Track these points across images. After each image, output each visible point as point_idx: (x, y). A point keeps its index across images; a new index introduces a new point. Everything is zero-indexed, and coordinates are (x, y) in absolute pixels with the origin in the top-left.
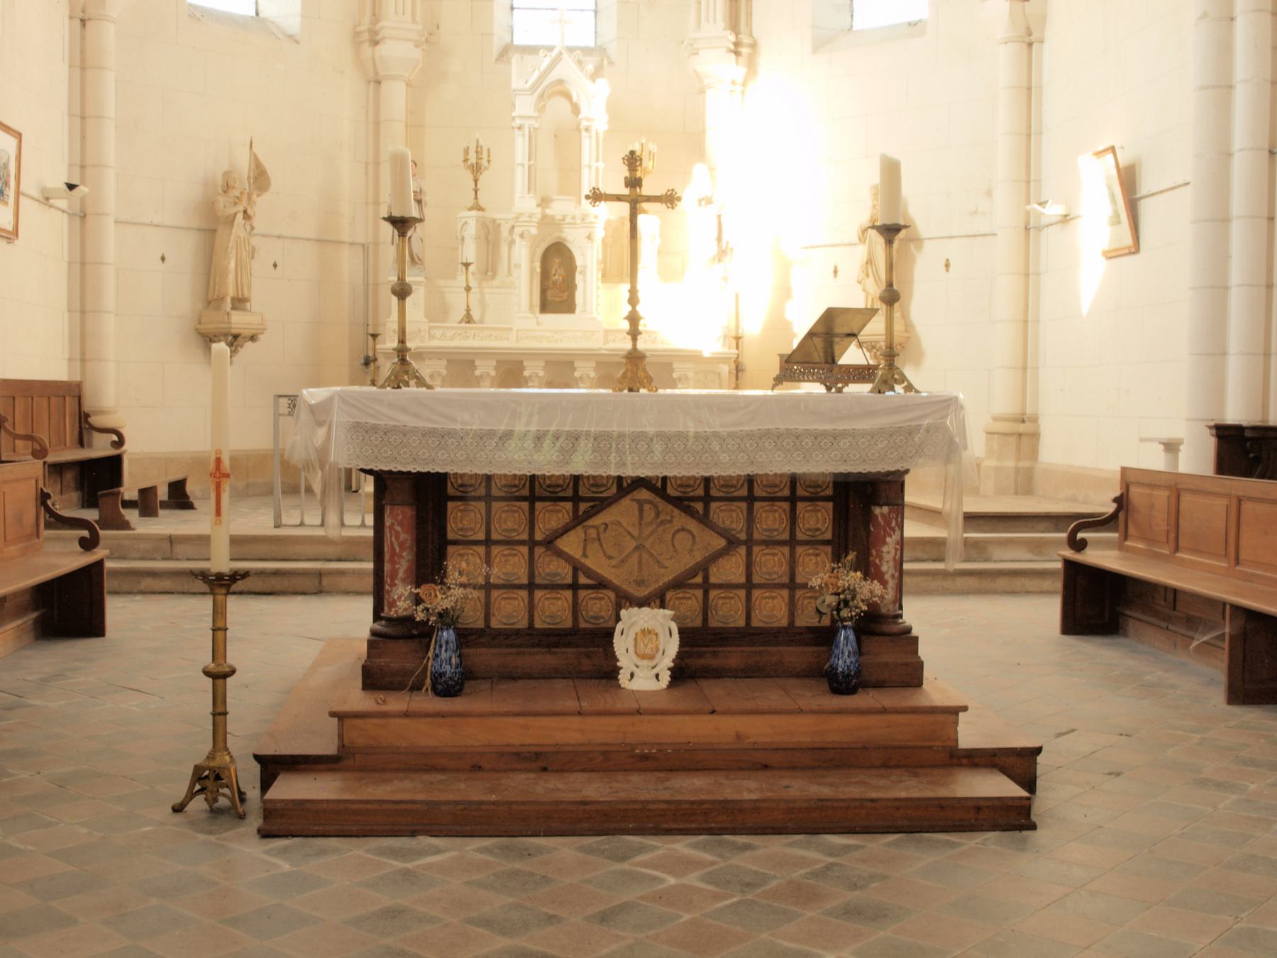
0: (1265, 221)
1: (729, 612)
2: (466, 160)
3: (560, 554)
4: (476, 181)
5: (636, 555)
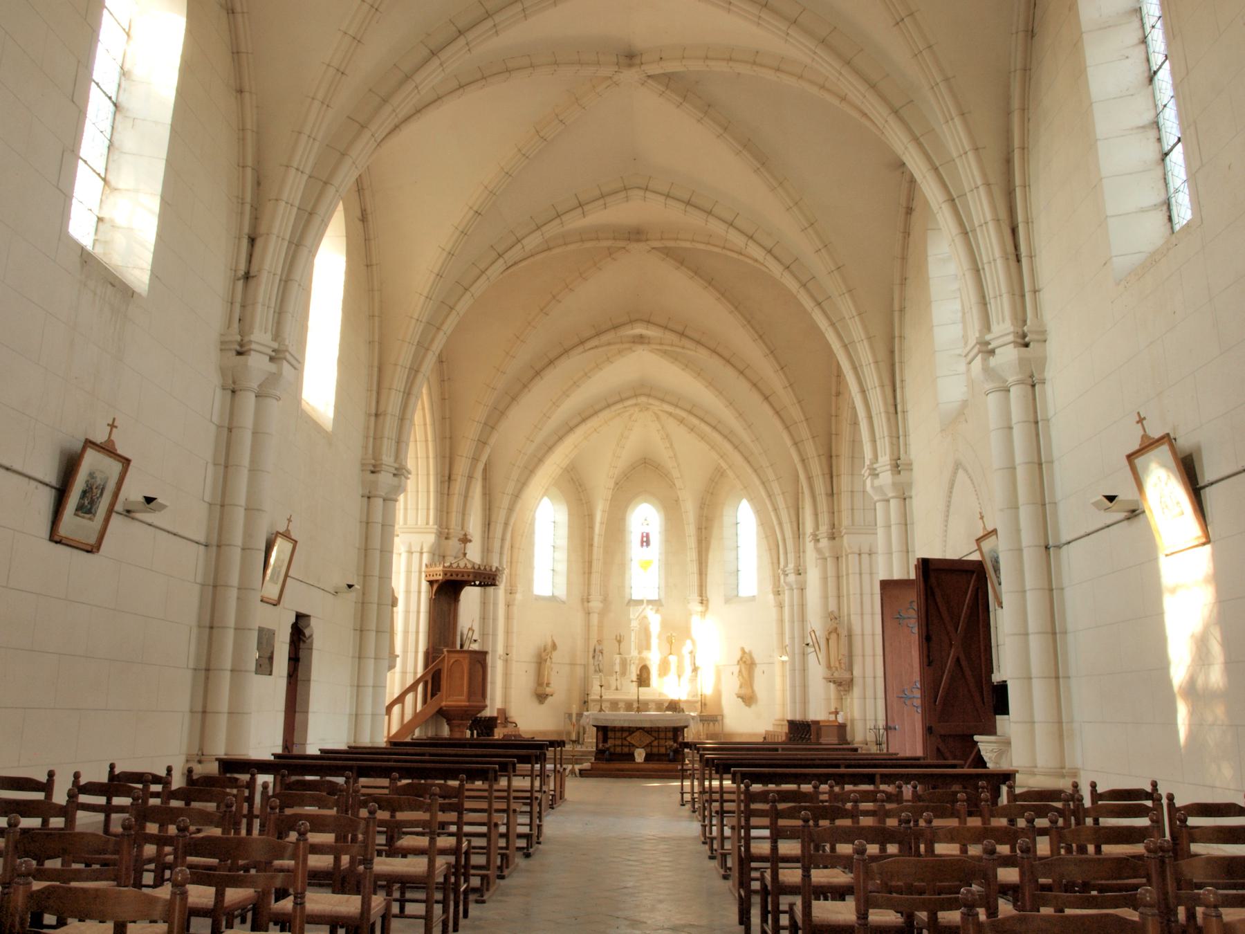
1: (655, 750)
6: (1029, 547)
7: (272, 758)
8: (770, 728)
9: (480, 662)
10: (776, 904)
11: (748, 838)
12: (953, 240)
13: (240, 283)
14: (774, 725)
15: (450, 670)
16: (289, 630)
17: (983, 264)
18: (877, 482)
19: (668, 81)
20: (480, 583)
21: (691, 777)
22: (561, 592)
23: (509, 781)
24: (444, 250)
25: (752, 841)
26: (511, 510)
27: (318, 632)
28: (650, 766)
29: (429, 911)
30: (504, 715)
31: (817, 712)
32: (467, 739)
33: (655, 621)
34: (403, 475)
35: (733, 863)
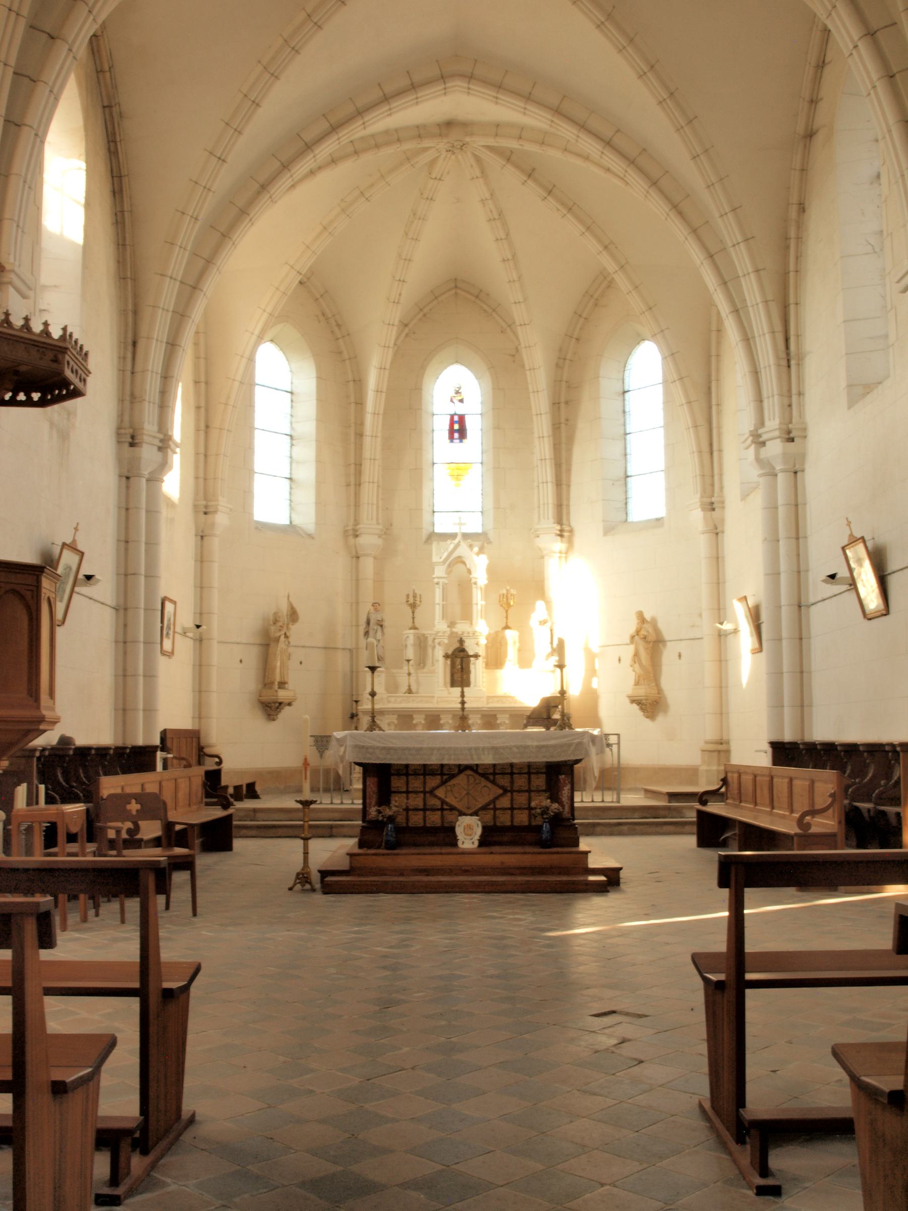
0: (798, 640)
1: (504, 819)
2: (408, 601)
3: (436, 796)
4: (413, 613)
5: (466, 797)
9: (22, 597)
22: (306, 519)
28: (497, 857)
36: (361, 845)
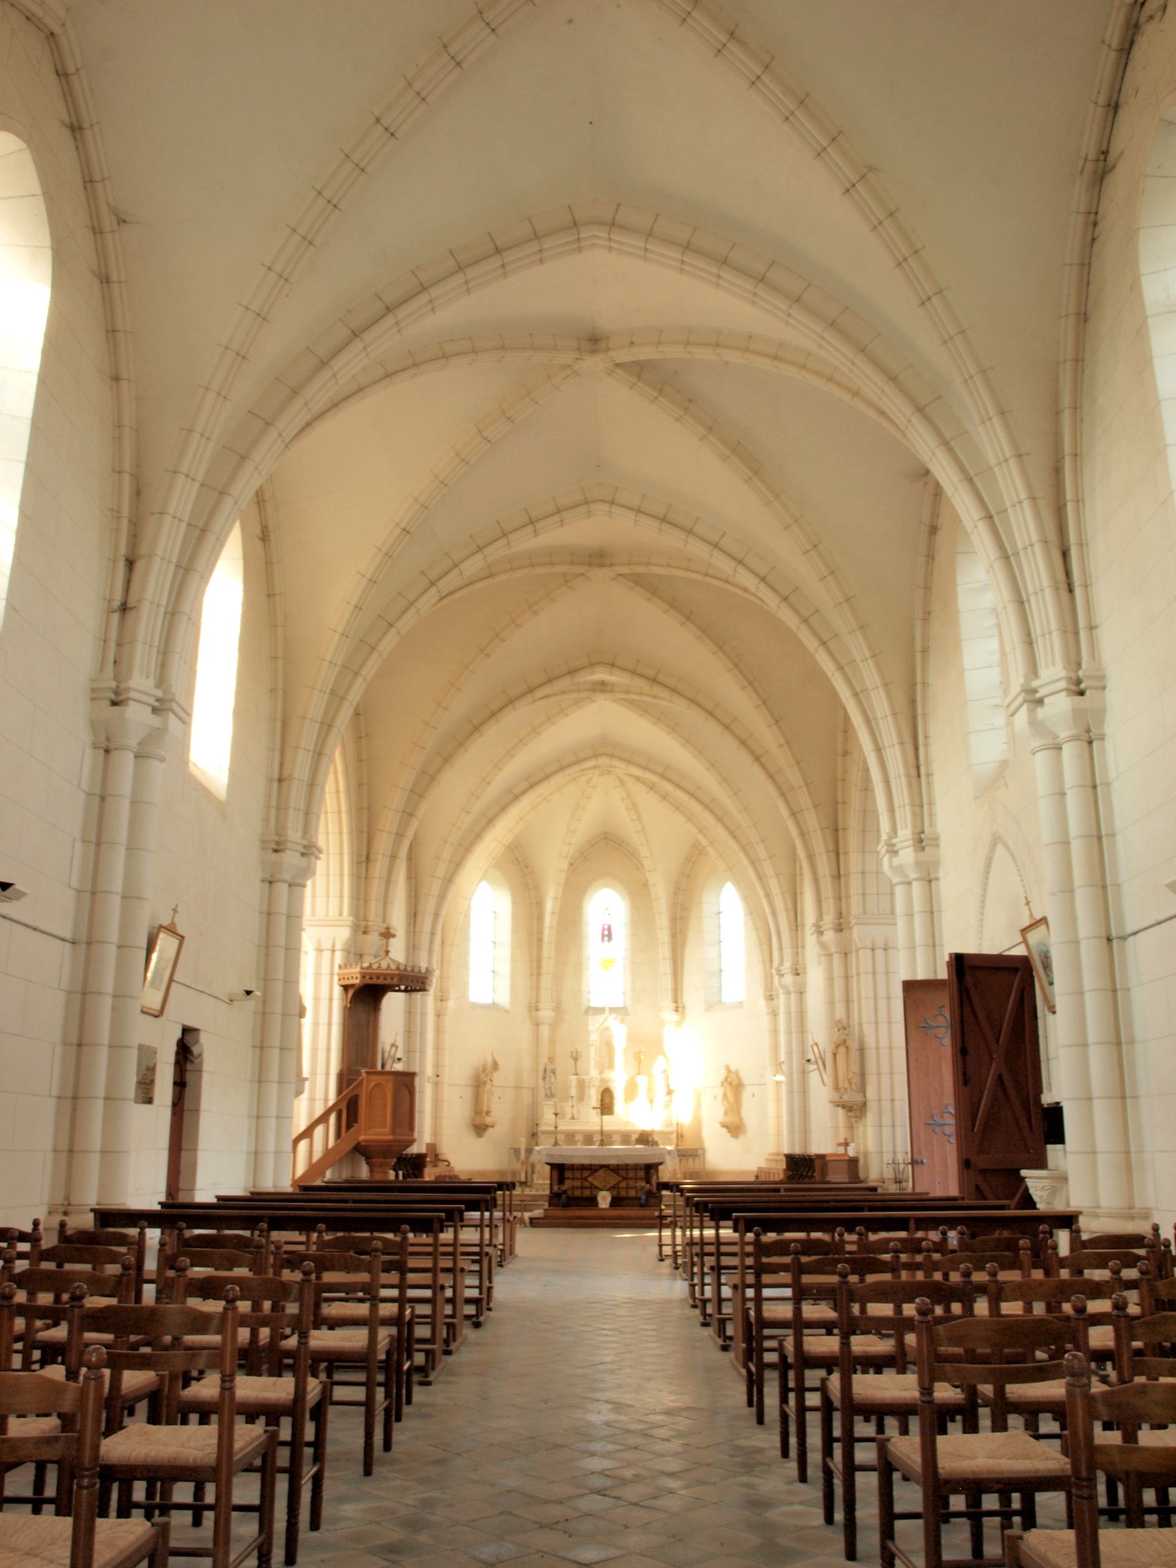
1: (623, 1193)
6: (1088, 938)
7: (158, 1207)
8: (763, 1164)
10: (800, 1379)
11: (759, 1300)
12: (991, 566)
13: (116, 617)
14: (767, 1160)
15: (370, 1095)
16: (174, 1048)
17: (1028, 595)
18: (896, 861)
19: (639, 371)
20: (407, 987)
21: (672, 1226)
22: (503, 998)
23: (456, 1233)
24: (363, 576)
25: (764, 1302)
26: (442, 897)
27: (208, 1049)
28: (617, 1212)
29: (370, 1396)
30: (434, 1155)
31: (821, 1144)
32: (391, 1182)
33: (619, 1033)
34: (312, 854)
35: (736, 1330)
36: (550, 1206)
